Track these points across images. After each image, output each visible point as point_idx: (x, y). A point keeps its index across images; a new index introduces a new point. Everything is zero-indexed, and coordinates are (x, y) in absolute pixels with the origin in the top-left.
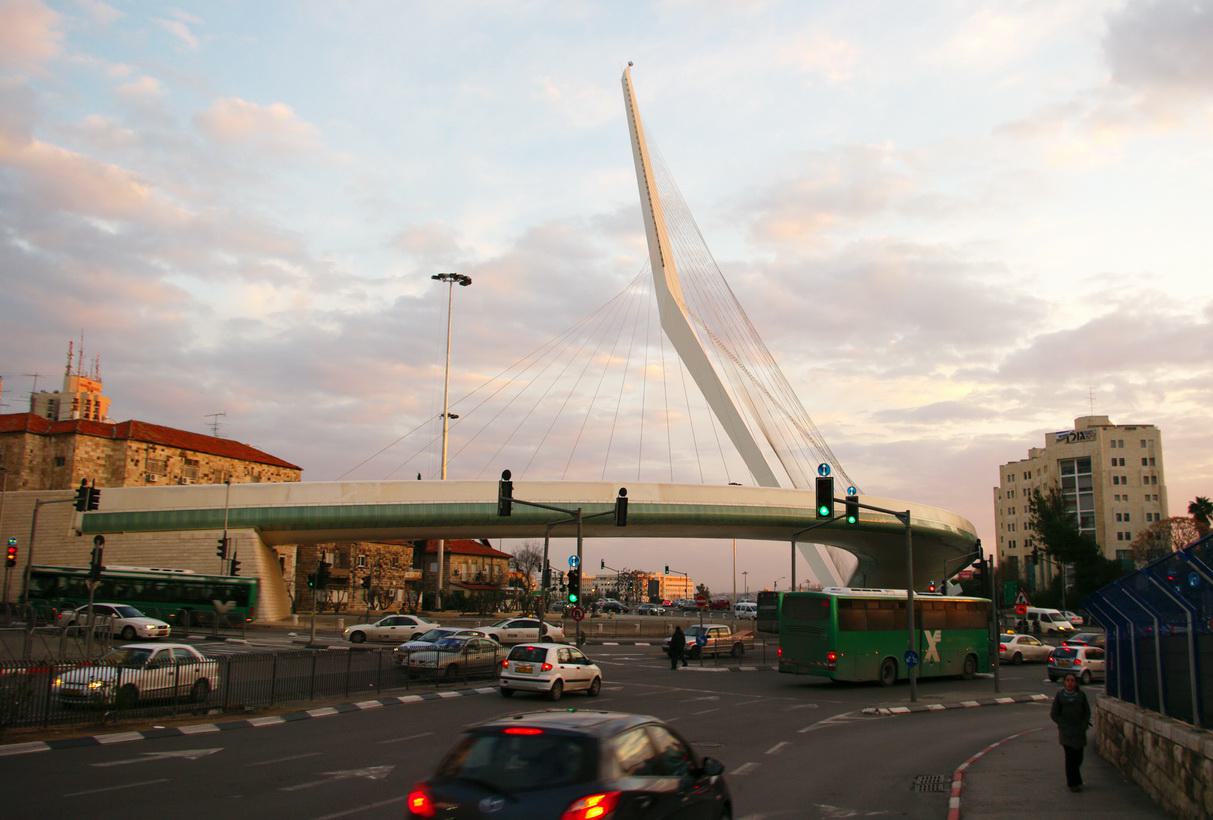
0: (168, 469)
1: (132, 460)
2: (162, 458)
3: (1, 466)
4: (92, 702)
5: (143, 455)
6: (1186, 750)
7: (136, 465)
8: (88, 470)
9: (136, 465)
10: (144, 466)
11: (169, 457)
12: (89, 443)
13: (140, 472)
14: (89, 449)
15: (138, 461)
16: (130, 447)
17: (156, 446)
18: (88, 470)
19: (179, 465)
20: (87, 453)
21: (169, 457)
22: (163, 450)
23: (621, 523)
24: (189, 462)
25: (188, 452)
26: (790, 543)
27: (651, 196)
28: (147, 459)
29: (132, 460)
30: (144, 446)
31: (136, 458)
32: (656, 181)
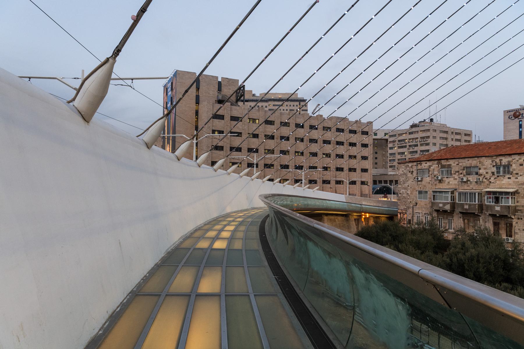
0: (430, 173)
1: (410, 172)
2: (426, 168)
3: (523, 187)
4: (416, 226)
5: (415, 168)
6: (414, 249)
7: (412, 174)
8: (403, 179)
9: (412, 174)
10: (416, 174)
11: (430, 166)
12: (403, 167)
13: (414, 177)
14: (403, 170)
15: (412, 172)
16: (408, 166)
17: (422, 162)
18: (403, 179)
19: (436, 169)
20: (403, 171)
21: (430, 166)
22: (426, 163)
23: (240, 135)
24: (443, 166)
25: (443, 161)
26: (111, 81)
27: (314, 309)
28: (417, 170)
29: (410, 172)
30: (415, 164)
31: (411, 170)
32: (111, 312)
